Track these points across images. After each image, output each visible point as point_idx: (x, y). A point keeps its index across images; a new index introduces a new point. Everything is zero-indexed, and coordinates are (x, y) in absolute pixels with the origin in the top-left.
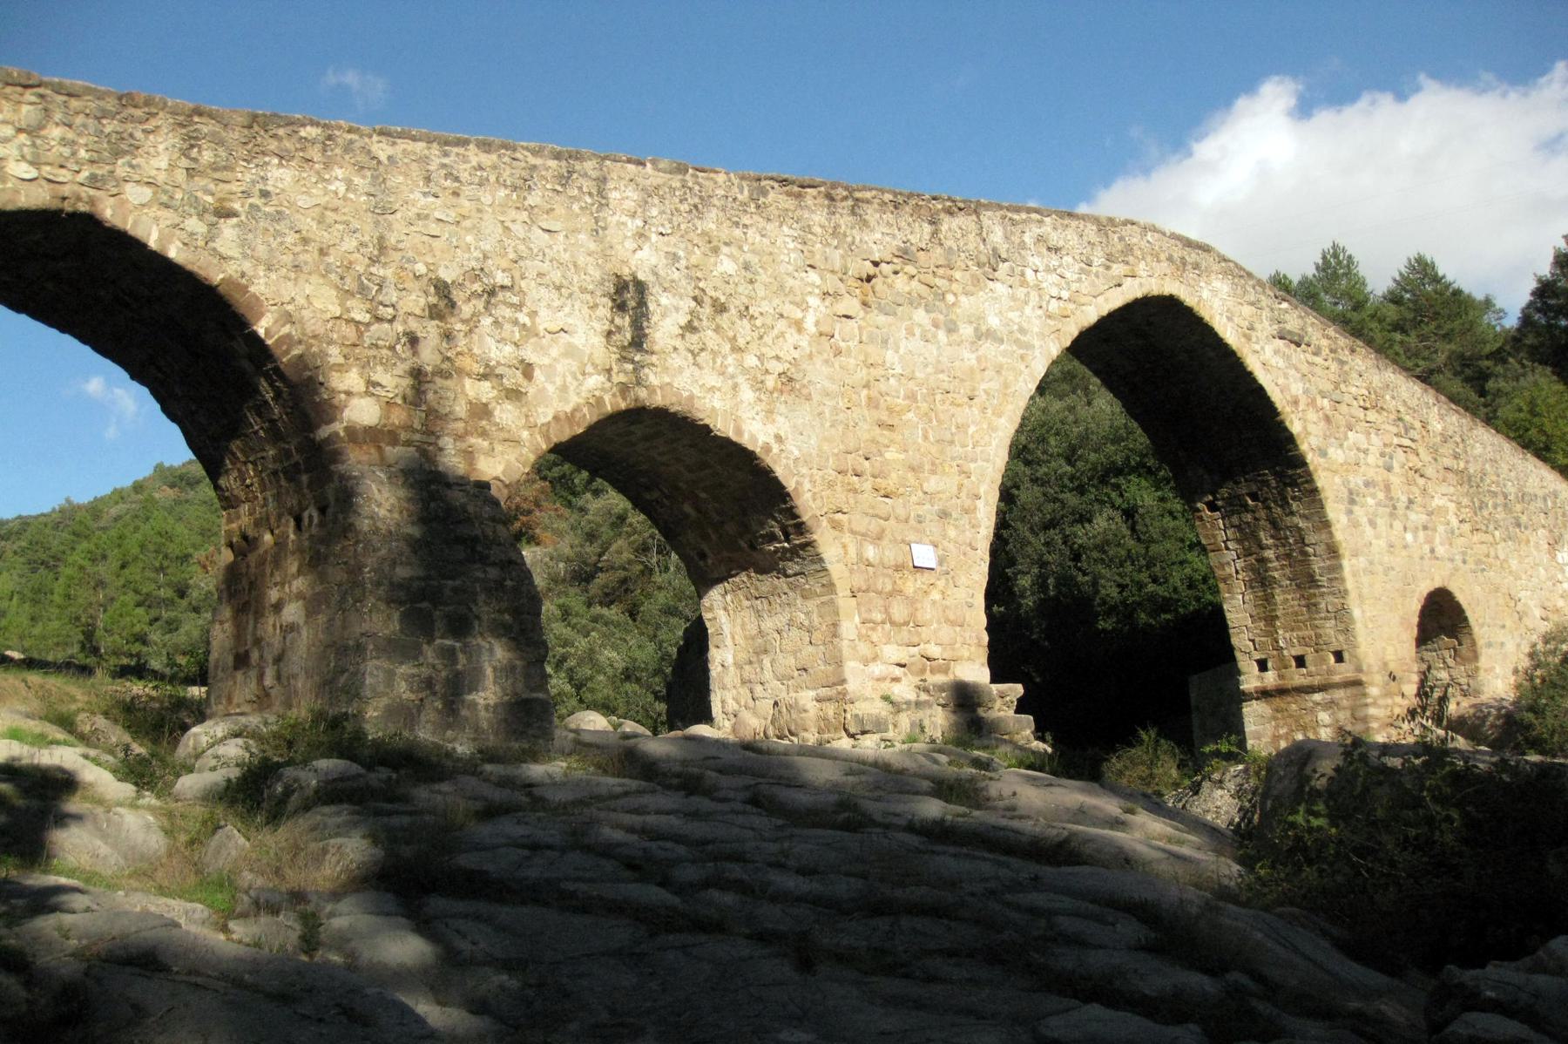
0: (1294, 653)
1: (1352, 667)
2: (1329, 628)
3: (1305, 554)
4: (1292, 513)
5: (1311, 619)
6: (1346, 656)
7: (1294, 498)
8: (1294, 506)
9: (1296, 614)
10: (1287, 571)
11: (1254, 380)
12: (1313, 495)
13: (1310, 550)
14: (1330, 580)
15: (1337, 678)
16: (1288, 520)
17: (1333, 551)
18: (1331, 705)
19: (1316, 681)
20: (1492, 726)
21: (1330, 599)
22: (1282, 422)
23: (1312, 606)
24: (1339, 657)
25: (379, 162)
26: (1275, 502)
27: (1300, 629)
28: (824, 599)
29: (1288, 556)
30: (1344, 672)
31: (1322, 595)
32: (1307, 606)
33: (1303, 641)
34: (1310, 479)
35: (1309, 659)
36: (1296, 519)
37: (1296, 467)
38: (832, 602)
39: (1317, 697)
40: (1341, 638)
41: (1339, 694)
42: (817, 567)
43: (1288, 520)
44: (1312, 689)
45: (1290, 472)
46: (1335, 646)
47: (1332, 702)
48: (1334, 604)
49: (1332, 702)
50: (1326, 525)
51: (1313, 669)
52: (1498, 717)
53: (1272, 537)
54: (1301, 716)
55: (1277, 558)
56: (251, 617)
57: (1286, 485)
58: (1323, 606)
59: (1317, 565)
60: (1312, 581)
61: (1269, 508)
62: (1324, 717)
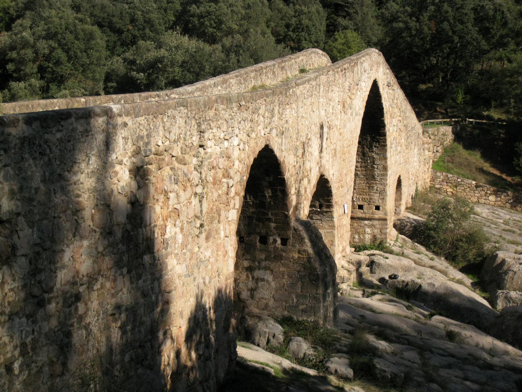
0: (359, 204)
1: (382, 213)
2: (376, 197)
3: (374, 168)
4: (373, 152)
5: (369, 192)
6: (381, 208)
7: (375, 147)
8: (374, 149)
9: (364, 189)
10: (364, 172)
11: (382, 105)
12: (384, 146)
13: (376, 166)
14: (382, 179)
15: (376, 216)
16: (370, 154)
17: (385, 168)
18: (372, 226)
19: (368, 216)
20: (407, 230)
21: (379, 186)
22: (384, 120)
23: (370, 187)
24: (377, 208)
25: (150, 28)
26: (367, 147)
27: (364, 195)
28: (329, 230)
29: (366, 167)
30: (379, 214)
31: (376, 184)
32: (369, 187)
33: (364, 200)
34: (385, 141)
35: (365, 207)
36: (373, 154)
37: (380, 136)
38: (332, 232)
39: (366, 222)
40: (380, 201)
41: (376, 223)
42: (330, 219)
43: (370, 154)
44: (365, 219)
45: (378, 137)
46: (377, 204)
47: (372, 225)
48: (380, 188)
49: (372, 225)
50: (385, 158)
51: (366, 211)
52: (411, 227)
53: (361, 159)
54: (358, 229)
55: (361, 167)
56: (144, 229)
57: (374, 141)
58: (375, 188)
59: (377, 172)
60: (373, 177)
61: (363, 148)
62: (368, 230)
